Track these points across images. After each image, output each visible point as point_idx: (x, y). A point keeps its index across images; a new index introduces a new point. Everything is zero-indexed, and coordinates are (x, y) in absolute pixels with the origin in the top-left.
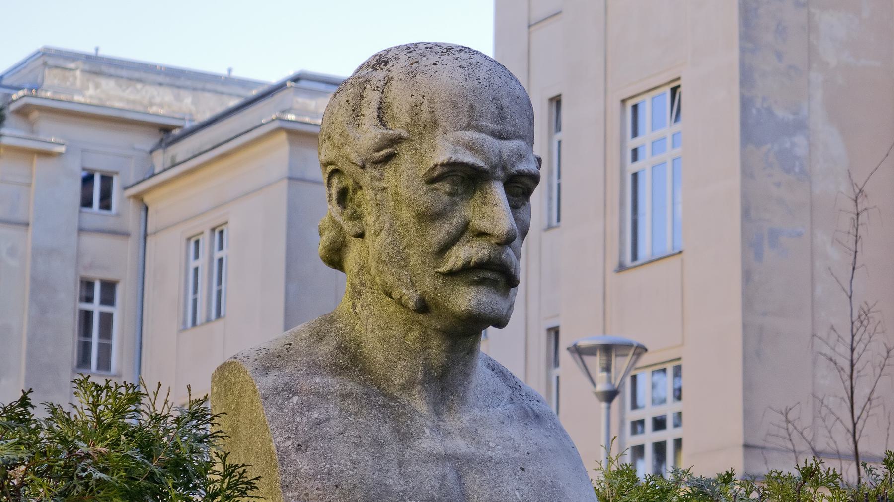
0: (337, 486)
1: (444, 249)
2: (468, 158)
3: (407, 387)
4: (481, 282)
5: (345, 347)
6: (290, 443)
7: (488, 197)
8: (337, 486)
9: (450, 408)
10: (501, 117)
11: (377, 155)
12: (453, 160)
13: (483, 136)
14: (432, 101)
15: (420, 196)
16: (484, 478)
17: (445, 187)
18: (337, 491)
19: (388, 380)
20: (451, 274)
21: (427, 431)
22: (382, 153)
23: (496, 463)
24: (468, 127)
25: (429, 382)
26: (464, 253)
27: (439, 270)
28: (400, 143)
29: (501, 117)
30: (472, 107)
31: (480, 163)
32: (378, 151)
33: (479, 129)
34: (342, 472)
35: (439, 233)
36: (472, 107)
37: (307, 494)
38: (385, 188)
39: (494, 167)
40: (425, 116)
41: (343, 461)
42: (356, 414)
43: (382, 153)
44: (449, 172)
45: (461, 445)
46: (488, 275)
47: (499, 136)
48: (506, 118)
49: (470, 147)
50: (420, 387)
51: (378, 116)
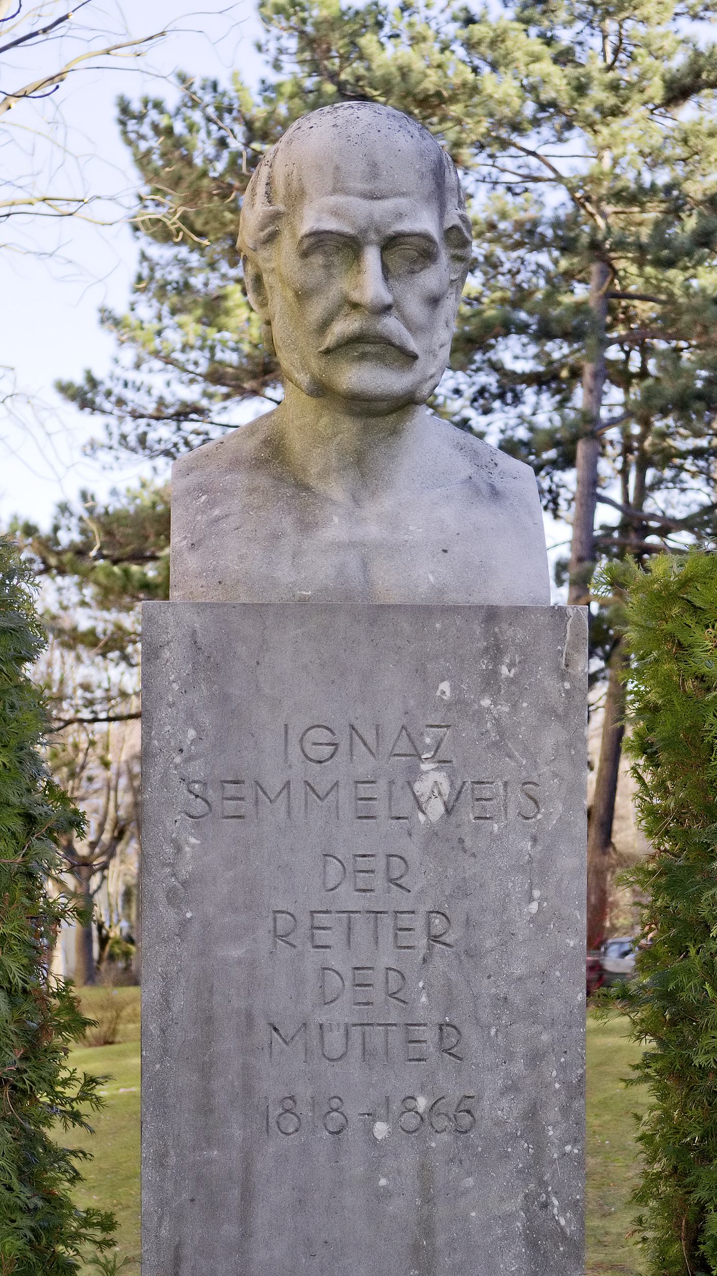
0: (220, 582)
1: (324, 326)
2: (331, 225)
3: (324, 475)
4: (363, 357)
5: (270, 441)
6: (185, 542)
7: (361, 264)
8: (220, 582)
9: (374, 493)
10: (374, 170)
11: (262, 234)
12: (315, 229)
13: (351, 198)
14: (300, 168)
15: (295, 273)
16: (392, 564)
17: (318, 260)
18: (220, 587)
19: (304, 470)
20: (328, 352)
21: (336, 519)
22: (267, 231)
23: (411, 547)
24: (334, 191)
25: (345, 469)
26: (344, 327)
27: (320, 349)
28: (280, 218)
29: (374, 170)
30: (337, 168)
31: (347, 229)
32: (262, 230)
33: (346, 192)
34: (228, 567)
35: (316, 310)
36: (337, 168)
37: (191, 593)
38: (274, 269)
39: (364, 231)
40: (295, 184)
41: (230, 557)
42: (259, 508)
43: (267, 231)
44: (316, 243)
45: (373, 531)
46: (369, 348)
47: (372, 196)
48: (381, 175)
49: (336, 213)
50: (335, 474)
51: (266, 193)
